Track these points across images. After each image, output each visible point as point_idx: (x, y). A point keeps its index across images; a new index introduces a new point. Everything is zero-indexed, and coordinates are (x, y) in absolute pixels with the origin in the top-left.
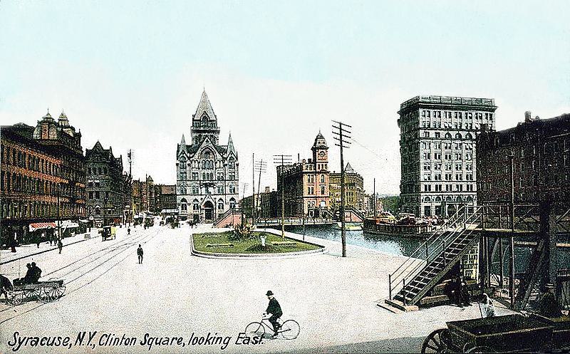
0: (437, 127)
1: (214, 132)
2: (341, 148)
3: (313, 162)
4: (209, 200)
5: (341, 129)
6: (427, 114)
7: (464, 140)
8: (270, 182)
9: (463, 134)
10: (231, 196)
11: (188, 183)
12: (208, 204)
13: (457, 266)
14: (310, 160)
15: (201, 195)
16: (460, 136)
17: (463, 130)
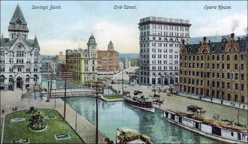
0: (160, 34)
1: (25, 31)
6: (171, 28)
7: (174, 42)
10: (10, 74)
15: (15, 73)
16: (172, 39)
17: (178, 37)
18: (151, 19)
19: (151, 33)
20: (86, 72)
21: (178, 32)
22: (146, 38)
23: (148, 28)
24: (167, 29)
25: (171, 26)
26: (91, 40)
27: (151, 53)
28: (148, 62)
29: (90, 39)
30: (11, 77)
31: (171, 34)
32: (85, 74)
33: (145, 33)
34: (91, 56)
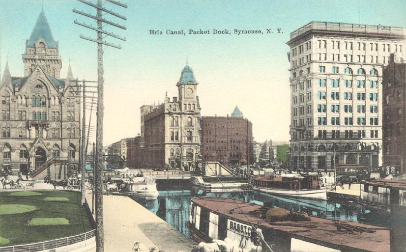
2: (100, 52)
3: (178, 101)
4: (39, 145)
5: (100, 21)
8: (134, 129)
9: (368, 69)
11: (13, 123)
12: (40, 151)
13: (59, 235)
14: (175, 98)
18: (315, 27)
19: (315, 57)
20: (175, 142)
21: (372, 52)
22: (305, 69)
23: (309, 47)
24: (377, 50)
25: (322, 39)
26: (184, 75)
27: (316, 102)
28: (310, 120)
29: (182, 73)
30: (24, 149)
31: (375, 59)
32: (173, 145)
33: (301, 60)
34: (186, 107)
